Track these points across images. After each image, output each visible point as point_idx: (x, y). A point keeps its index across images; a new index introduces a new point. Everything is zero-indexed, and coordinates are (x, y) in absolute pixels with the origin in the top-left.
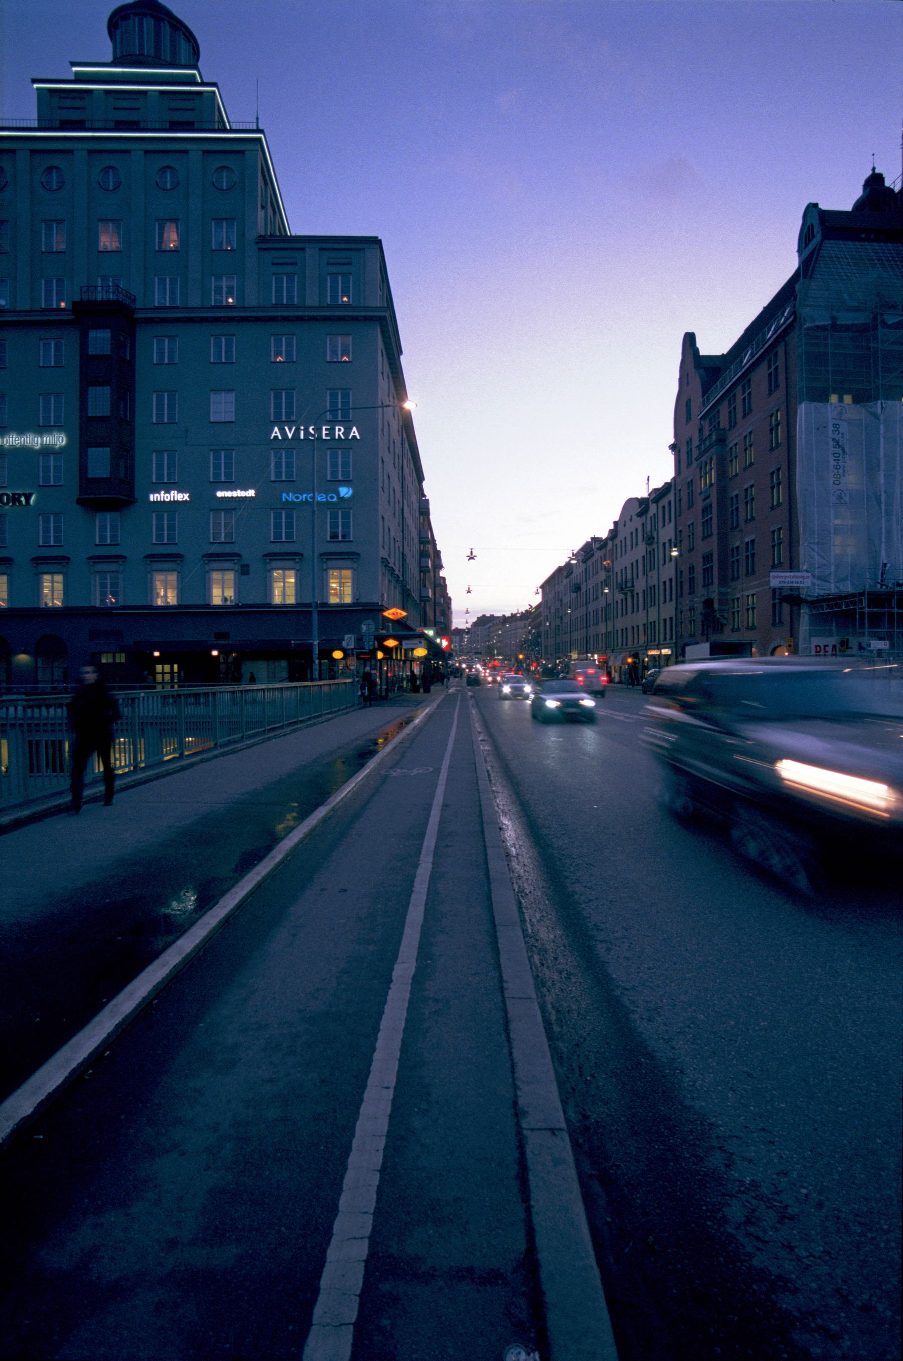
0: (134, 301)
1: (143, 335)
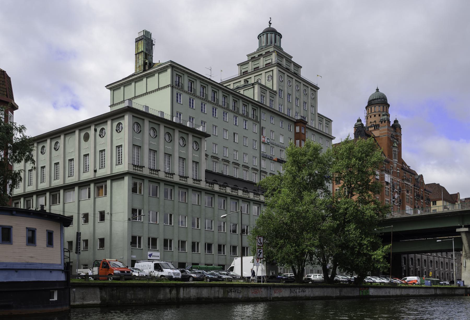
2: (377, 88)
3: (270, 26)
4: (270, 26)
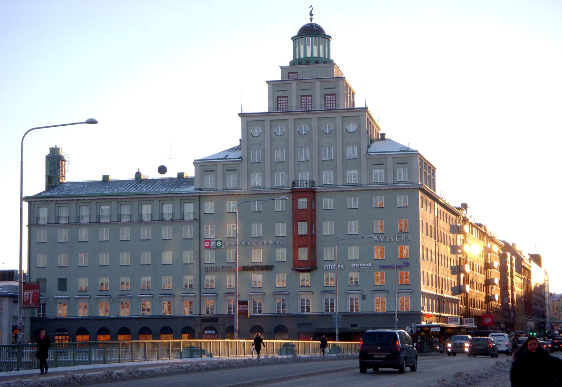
0: (314, 183)
1: (318, 197)
3: (311, 19)
4: (311, 19)
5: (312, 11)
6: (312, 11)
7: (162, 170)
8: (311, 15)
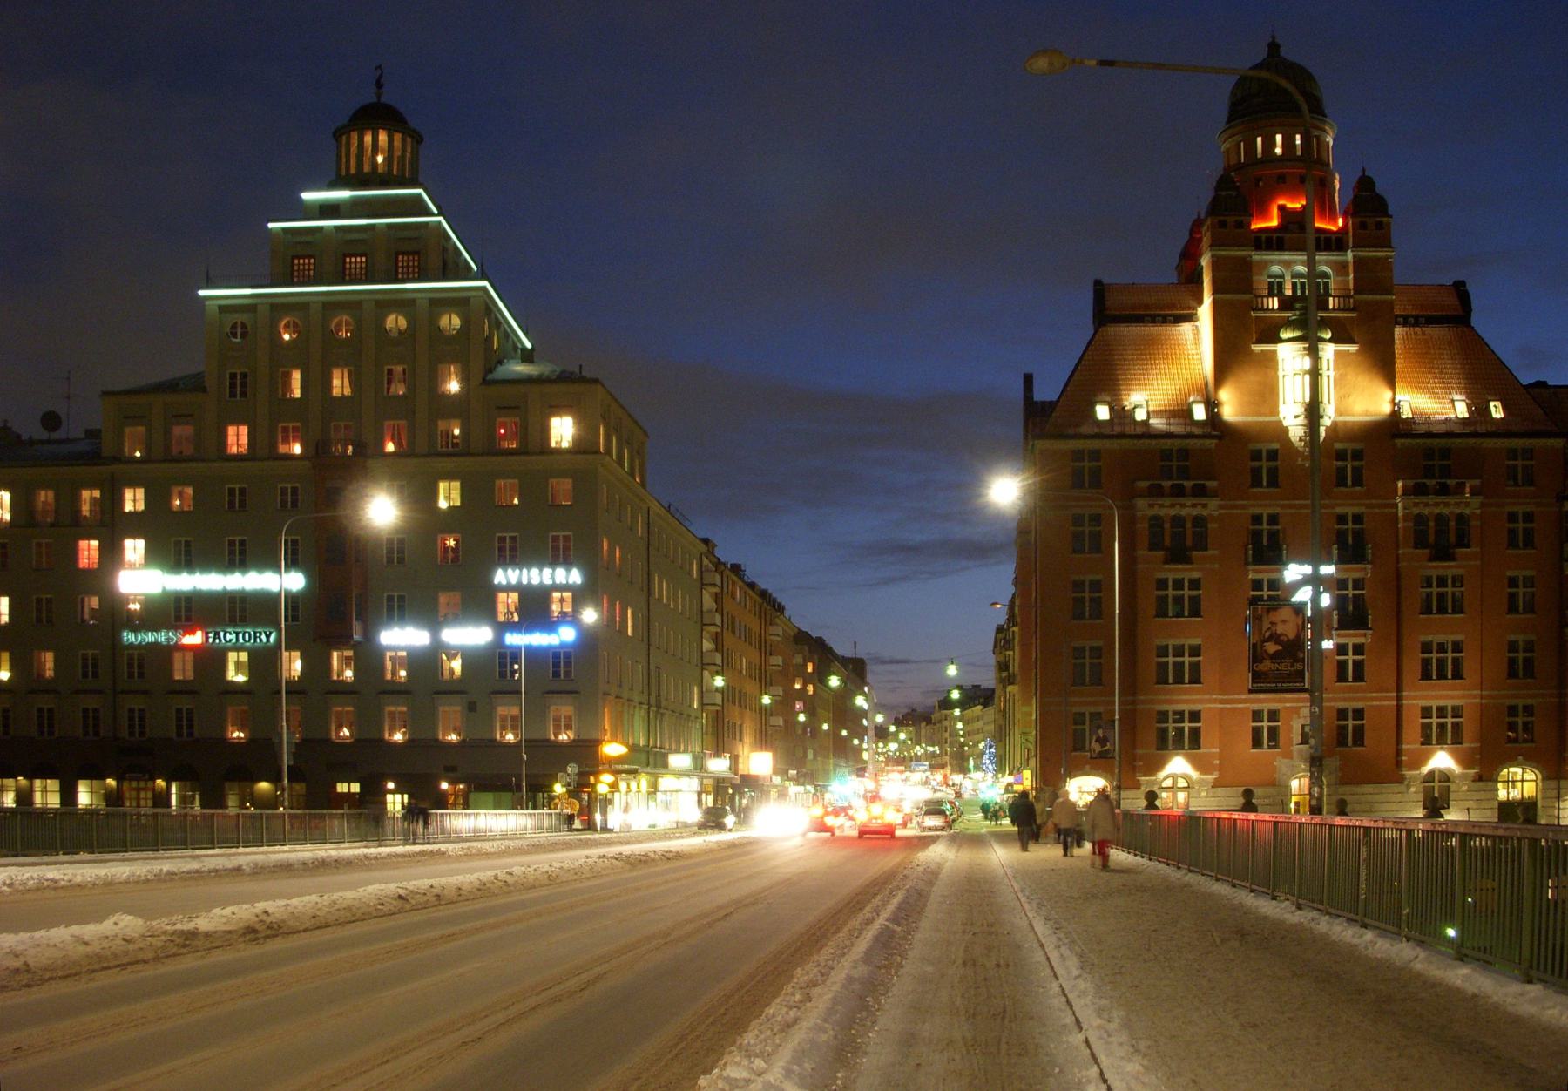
2: (1273, 37)
3: (379, 98)
4: (379, 98)
5: (381, 76)
6: (381, 76)
7: (51, 421)
8: (379, 85)
